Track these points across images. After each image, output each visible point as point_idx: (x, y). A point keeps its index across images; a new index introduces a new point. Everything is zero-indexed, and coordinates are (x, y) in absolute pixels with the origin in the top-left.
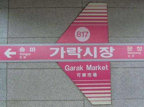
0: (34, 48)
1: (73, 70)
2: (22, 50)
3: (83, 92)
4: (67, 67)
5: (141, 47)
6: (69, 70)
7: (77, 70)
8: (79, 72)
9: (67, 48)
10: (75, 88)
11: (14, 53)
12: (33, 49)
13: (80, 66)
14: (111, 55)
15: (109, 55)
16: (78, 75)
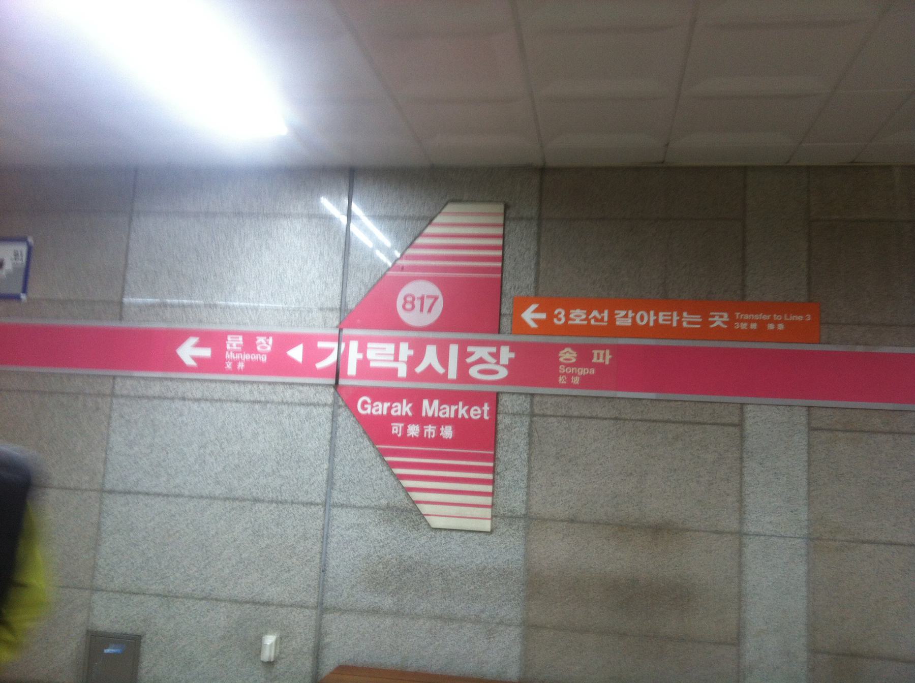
1: (380, 412)
2: (568, 356)
3: (407, 483)
4: (365, 403)
5: (271, 340)
6: (369, 411)
7: (393, 413)
8: (398, 419)
9: (370, 345)
10: (381, 468)
11: (206, 353)
12: (604, 355)
15: (494, 372)
16: (397, 429)
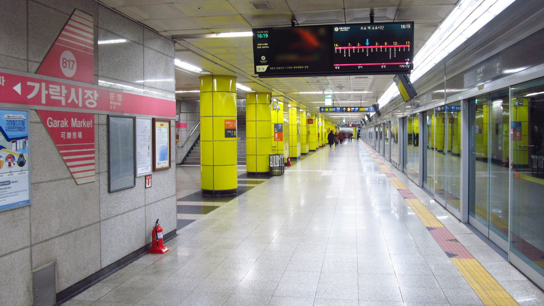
0: (3, 77)
3: (69, 164)
4: (50, 121)
9: (50, 86)
13: (65, 119)
14: (95, 105)
